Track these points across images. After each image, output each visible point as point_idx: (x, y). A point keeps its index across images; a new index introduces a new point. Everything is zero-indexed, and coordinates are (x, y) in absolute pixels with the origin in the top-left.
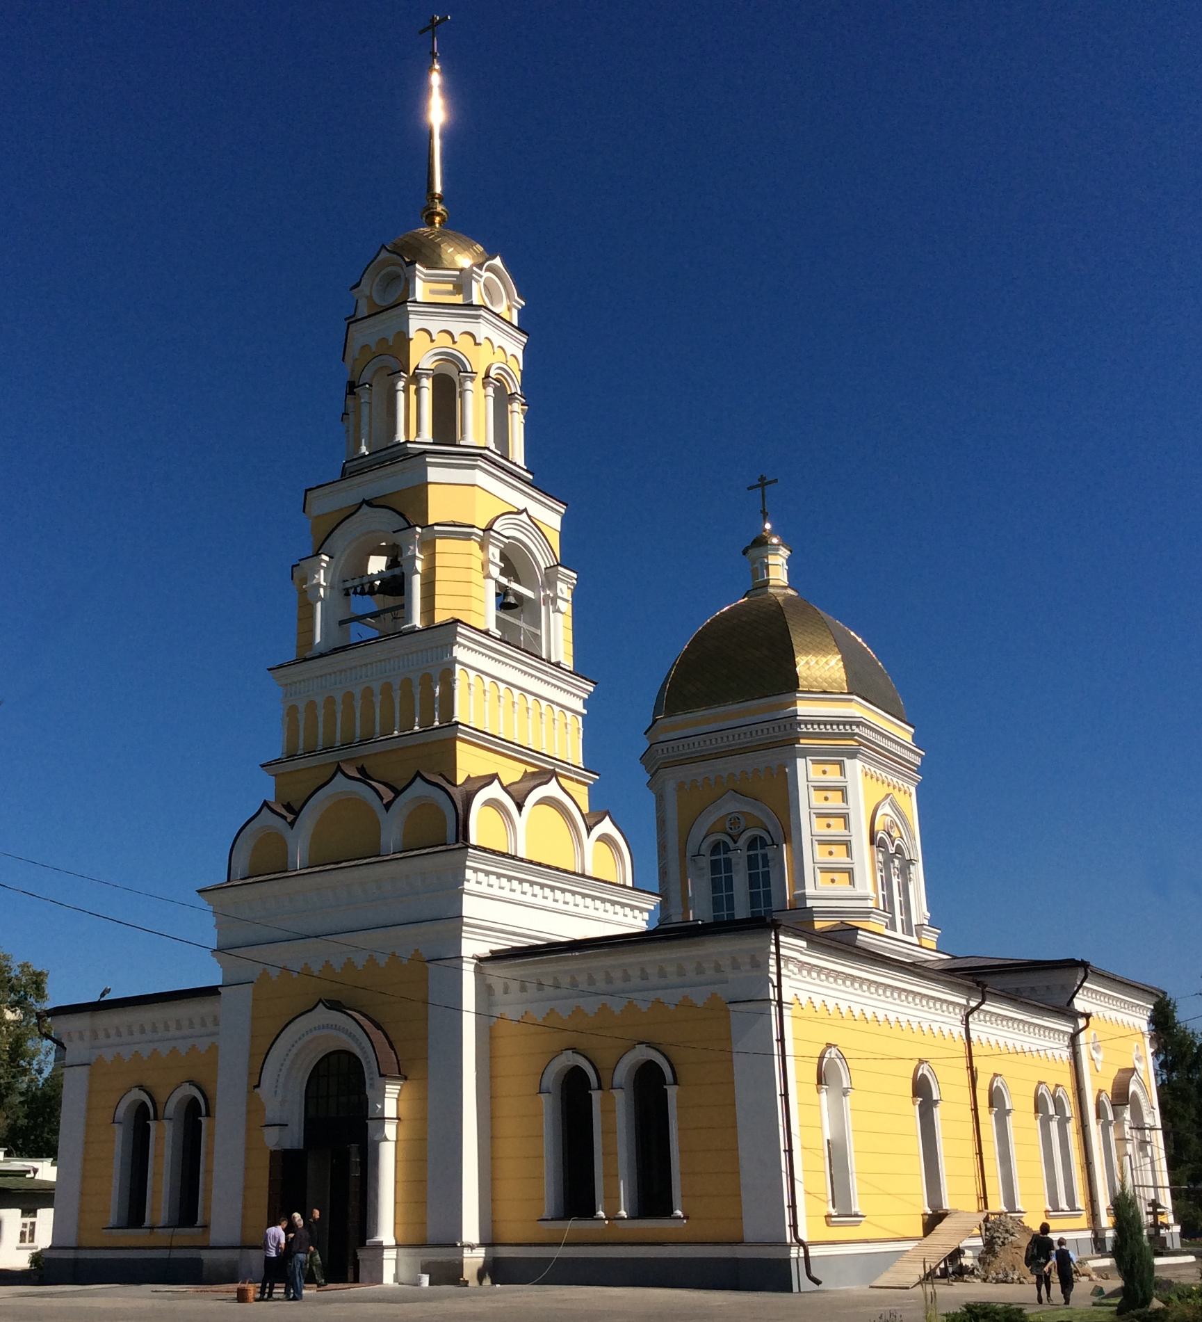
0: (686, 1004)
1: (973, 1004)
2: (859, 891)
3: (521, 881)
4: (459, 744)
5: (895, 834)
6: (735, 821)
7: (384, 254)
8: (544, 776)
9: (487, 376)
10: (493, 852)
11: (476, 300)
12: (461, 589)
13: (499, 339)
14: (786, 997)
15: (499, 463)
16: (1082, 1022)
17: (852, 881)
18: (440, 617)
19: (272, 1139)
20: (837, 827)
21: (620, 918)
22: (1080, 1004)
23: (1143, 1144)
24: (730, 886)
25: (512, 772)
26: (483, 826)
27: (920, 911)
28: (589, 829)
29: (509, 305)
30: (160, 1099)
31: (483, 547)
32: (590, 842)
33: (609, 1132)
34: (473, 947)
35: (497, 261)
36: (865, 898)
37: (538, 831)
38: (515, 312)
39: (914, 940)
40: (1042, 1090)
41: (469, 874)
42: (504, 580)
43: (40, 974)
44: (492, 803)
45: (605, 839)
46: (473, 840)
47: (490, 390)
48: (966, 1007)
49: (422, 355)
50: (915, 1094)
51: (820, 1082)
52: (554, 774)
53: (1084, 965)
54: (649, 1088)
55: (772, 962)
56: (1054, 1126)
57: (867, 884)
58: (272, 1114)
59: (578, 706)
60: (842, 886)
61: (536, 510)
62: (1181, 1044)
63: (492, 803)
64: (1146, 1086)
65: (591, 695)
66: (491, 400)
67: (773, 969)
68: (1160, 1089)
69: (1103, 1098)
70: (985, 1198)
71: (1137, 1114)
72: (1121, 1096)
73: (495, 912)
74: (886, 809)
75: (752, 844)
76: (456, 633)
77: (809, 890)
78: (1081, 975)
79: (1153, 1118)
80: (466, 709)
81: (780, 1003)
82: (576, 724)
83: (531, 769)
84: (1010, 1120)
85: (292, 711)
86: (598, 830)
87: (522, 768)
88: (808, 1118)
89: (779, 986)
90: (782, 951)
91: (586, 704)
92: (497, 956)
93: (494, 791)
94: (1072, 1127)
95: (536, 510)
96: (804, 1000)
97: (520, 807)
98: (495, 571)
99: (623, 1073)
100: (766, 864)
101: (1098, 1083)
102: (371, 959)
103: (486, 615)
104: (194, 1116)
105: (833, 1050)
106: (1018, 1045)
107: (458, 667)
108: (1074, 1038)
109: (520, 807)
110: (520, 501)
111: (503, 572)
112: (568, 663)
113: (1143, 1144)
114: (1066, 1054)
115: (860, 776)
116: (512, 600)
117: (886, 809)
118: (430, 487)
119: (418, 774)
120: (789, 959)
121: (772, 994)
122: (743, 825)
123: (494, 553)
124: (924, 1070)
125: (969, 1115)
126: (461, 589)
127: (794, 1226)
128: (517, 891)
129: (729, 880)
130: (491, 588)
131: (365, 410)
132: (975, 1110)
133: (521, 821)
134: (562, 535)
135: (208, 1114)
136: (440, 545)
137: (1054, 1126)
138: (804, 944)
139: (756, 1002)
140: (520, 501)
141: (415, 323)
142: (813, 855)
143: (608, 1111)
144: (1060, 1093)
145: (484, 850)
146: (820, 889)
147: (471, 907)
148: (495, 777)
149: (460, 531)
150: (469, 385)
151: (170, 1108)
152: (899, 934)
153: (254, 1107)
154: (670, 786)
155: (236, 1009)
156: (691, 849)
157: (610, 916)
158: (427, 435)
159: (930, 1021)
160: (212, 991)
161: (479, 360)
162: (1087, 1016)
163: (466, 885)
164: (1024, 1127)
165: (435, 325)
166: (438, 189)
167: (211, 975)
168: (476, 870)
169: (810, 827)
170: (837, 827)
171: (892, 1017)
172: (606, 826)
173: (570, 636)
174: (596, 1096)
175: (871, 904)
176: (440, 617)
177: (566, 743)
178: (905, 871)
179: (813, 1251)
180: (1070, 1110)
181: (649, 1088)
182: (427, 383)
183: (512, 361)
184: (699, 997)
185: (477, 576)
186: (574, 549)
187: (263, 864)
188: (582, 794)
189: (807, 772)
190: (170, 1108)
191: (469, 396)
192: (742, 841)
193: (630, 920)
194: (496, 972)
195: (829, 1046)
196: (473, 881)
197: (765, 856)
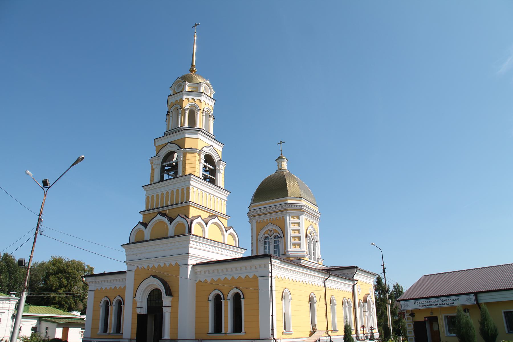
0: (247, 277)
1: (326, 277)
2: (302, 250)
3: (206, 244)
4: (190, 207)
5: (313, 235)
6: (271, 231)
7: (178, 79)
8: (214, 216)
9: (203, 110)
10: (198, 236)
11: (201, 91)
12: (193, 165)
13: (207, 101)
14: (274, 275)
15: (206, 134)
16: (356, 282)
17: (300, 247)
18: (187, 173)
19: (138, 311)
20: (297, 234)
21: (229, 254)
22: (355, 278)
23: (370, 315)
24: (269, 249)
25: (205, 215)
26: (195, 229)
27: (318, 255)
28: (226, 231)
29: (211, 92)
30: (112, 300)
31: (199, 155)
32: (226, 235)
33: (226, 311)
34: (192, 262)
35: (208, 82)
36: (304, 251)
37: (211, 231)
38: (212, 95)
39: (317, 262)
40: (345, 299)
41: (191, 242)
42: (205, 164)
43: (92, 268)
44: (199, 223)
45: (231, 234)
46: (193, 233)
47: (204, 114)
48: (324, 278)
49: (186, 105)
50: (310, 300)
51: (282, 298)
52: (216, 216)
53: (357, 267)
54: (237, 299)
55: (270, 266)
56: (347, 309)
57: (304, 248)
58: (139, 305)
59: (225, 198)
60: (297, 249)
61: (215, 146)
62: (383, 288)
63: (199, 223)
64: (372, 299)
65: (229, 195)
66: (204, 117)
67: (270, 268)
68: (376, 300)
69: (360, 301)
70: (327, 327)
71: (369, 308)
72: (365, 301)
73: (198, 252)
74: (310, 228)
75: (275, 237)
76: (191, 177)
77: (289, 249)
78: (356, 270)
79: (373, 306)
80: (193, 197)
81: (271, 277)
82: (224, 203)
83: (211, 215)
84: (336, 307)
85: (148, 198)
86: (229, 232)
87: (208, 214)
88: (278, 307)
89: (272, 272)
90: (272, 263)
91: (227, 198)
92: (198, 264)
93: (199, 220)
94: (352, 309)
95: (215, 146)
96: (279, 277)
97: (206, 224)
98: (202, 161)
99: (230, 296)
100: (278, 243)
101: (359, 298)
102: (165, 265)
103: (199, 172)
104: (120, 304)
105: (287, 290)
106: (339, 288)
107: (191, 187)
108: (354, 286)
109: (206, 224)
110: (211, 143)
111: (205, 162)
112: (223, 187)
113: (370, 315)
114: (351, 290)
115: (304, 219)
116: (208, 169)
117: (310, 228)
118: (186, 139)
119: (179, 215)
120: (275, 265)
121: (270, 275)
122: (273, 232)
123: (203, 156)
124: (312, 295)
125: (324, 306)
126: (193, 165)
127: (273, 335)
128: (204, 247)
129: (269, 247)
130: (202, 166)
131: (171, 118)
132: (326, 305)
133: (207, 228)
134: (222, 153)
135: (124, 304)
136: (187, 154)
137: (347, 309)
138: (279, 261)
139: (268, 276)
140: (211, 143)
141: (185, 97)
142: (290, 241)
143: (226, 306)
144: (349, 300)
145: (195, 235)
146: (291, 249)
147: (191, 251)
148: (199, 216)
149: (193, 150)
150: (199, 113)
151: (114, 303)
152: (313, 261)
153: (134, 303)
154: (254, 222)
155: (130, 278)
156: (259, 239)
157: (226, 253)
158: (186, 125)
159: (316, 281)
160: (124, 272)
161: (203, 106)
162: (357, 281)
163: (190, 245)
164: (339, 309)
165: (190, 97)
166: (194, 64)
167: (124, 268)
168: (193, 241)
169: (290, 233)
170: (297, 234)
171: (304, 281)
172: (231, 231)
173: (223, 179)
174: (223, 302)
175: (305, 253)
176: (187, 173)
177: (222, 208)
178: (315, 245)
179: (332, 337)
180: (352, 305)
181: (237, 299)
182: (187, 112)
183: (211, 107)
184: (251, 276)
185: (197, 162)
186: (225, 157)
187: (137, 240)
188: (225, 223)
189: (289, 219)
190: (114, 303)
191: (198, 115)
192: (272, 236)
193: (231, 255)
194: (198, 269)
195: (285, 288)
196: (192, 244)
197: (269, 242)
